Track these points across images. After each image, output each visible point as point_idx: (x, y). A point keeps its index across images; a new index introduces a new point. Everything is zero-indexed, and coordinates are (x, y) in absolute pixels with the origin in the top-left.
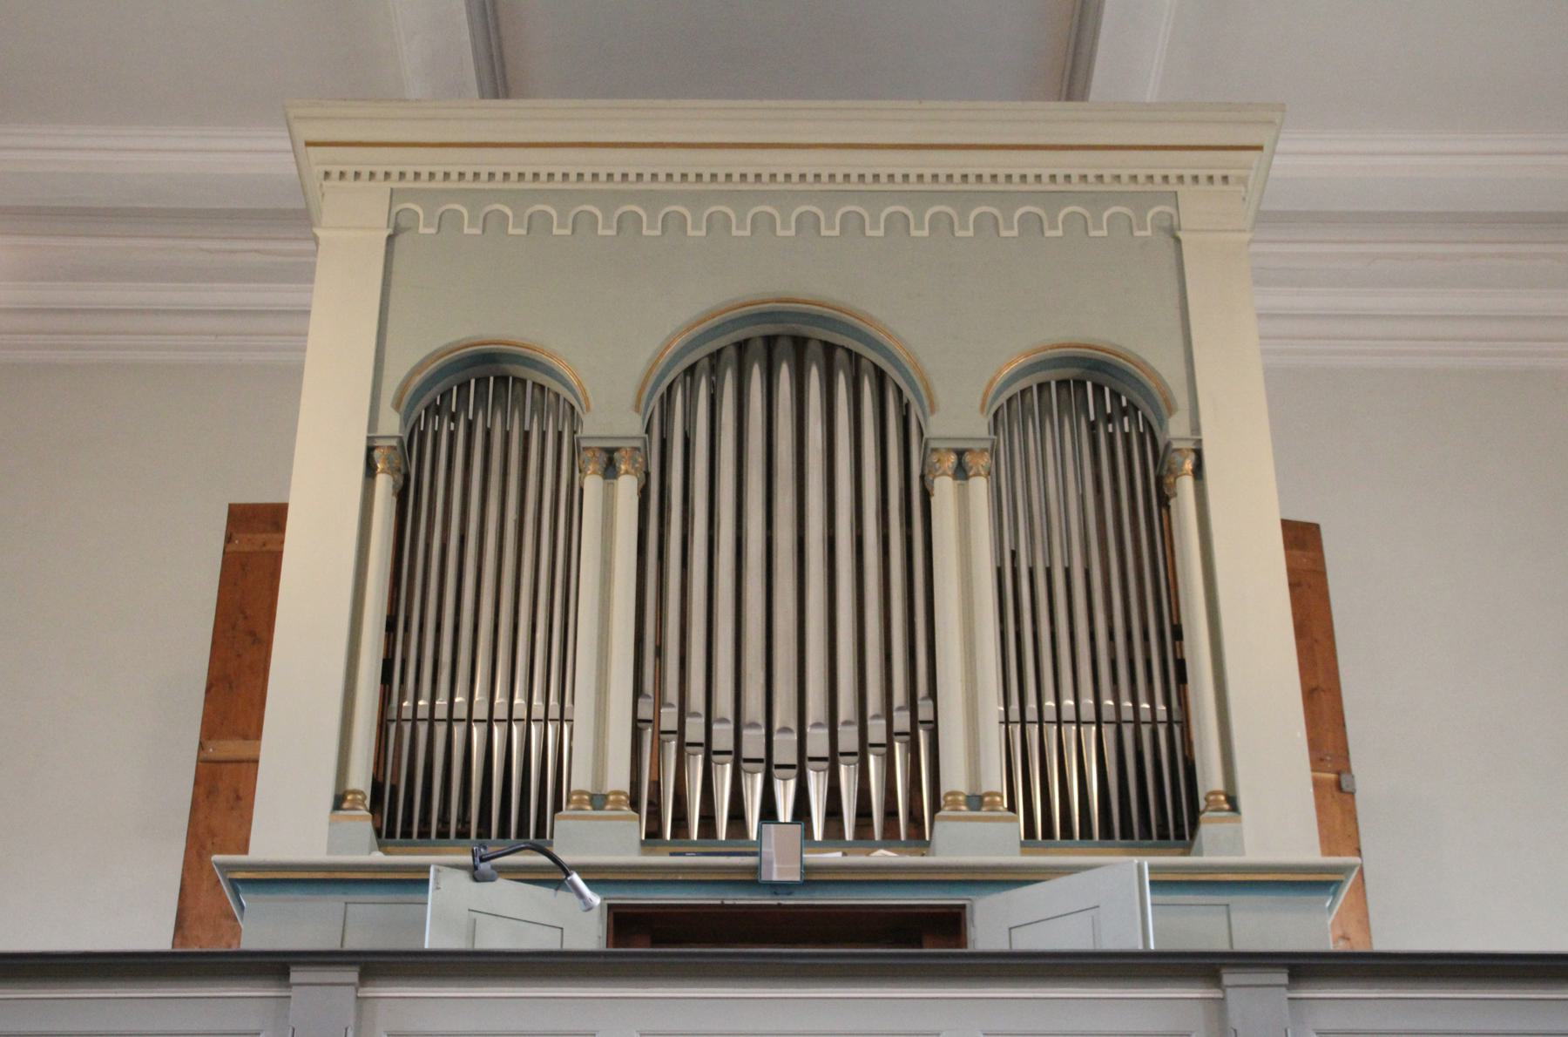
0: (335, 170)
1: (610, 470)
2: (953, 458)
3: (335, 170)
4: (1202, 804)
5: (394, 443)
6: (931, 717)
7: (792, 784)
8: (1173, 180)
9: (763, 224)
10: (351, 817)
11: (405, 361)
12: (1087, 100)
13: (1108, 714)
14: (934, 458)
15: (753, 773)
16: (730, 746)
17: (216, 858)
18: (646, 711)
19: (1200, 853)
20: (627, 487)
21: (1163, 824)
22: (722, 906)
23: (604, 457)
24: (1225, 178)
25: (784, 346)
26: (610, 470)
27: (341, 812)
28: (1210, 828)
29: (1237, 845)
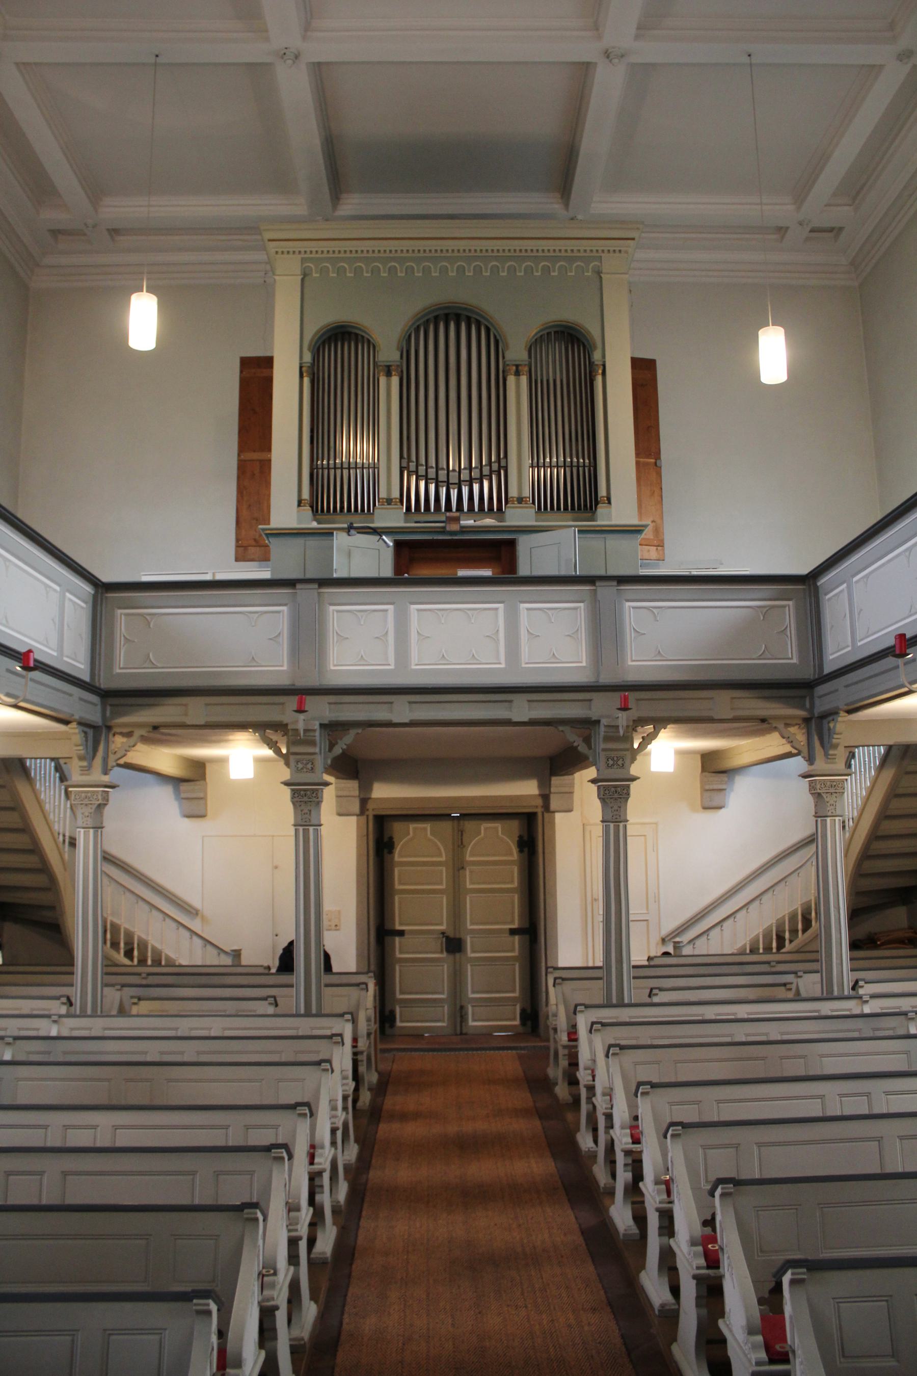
0: (280, 250)
1: (389, 374)
2: (514, 368)
3: (280, 250)
5: (309, 365)
6: (505, 465)
7: (456, 491)
8: (600, 251)
9: (443, 270)
10: (304, 510)
11: (311, 331)
13: (568, 464)
15: (443, 487)
16: (434, 477)
17: (261, 527)
18: (404, 464)
19: (596, 521)
20: (395, 380)
21: (585, 505)
22: (433, 539)
23: (386, 369)
26: (389, 374)
27: (301, 508)
28: (601, 510)
29: (609, 517)
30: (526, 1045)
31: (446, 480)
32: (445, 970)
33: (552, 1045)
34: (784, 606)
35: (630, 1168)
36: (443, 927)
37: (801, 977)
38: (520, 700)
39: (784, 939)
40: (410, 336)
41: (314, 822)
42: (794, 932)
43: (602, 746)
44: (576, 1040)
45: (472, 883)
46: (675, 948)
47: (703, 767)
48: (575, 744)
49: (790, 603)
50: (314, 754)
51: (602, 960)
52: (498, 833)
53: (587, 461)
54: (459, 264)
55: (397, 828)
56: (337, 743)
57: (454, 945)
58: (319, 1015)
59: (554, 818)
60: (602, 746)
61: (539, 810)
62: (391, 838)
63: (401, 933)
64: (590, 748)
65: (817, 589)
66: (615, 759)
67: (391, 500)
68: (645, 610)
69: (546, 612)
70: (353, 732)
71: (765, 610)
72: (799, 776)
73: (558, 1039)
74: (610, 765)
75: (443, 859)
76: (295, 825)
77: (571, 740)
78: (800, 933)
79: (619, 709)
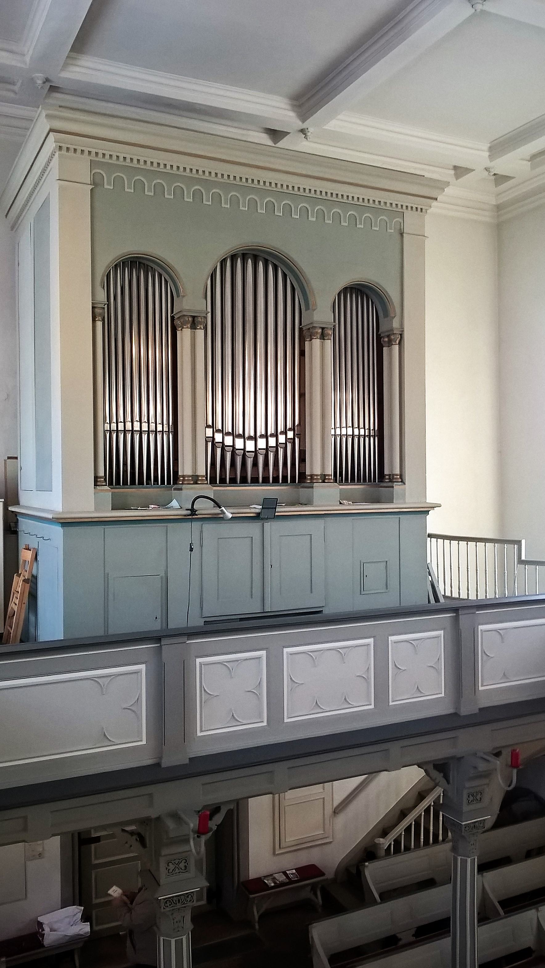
54: (250, 197)
68: (219, 665)
69: (498, 632)
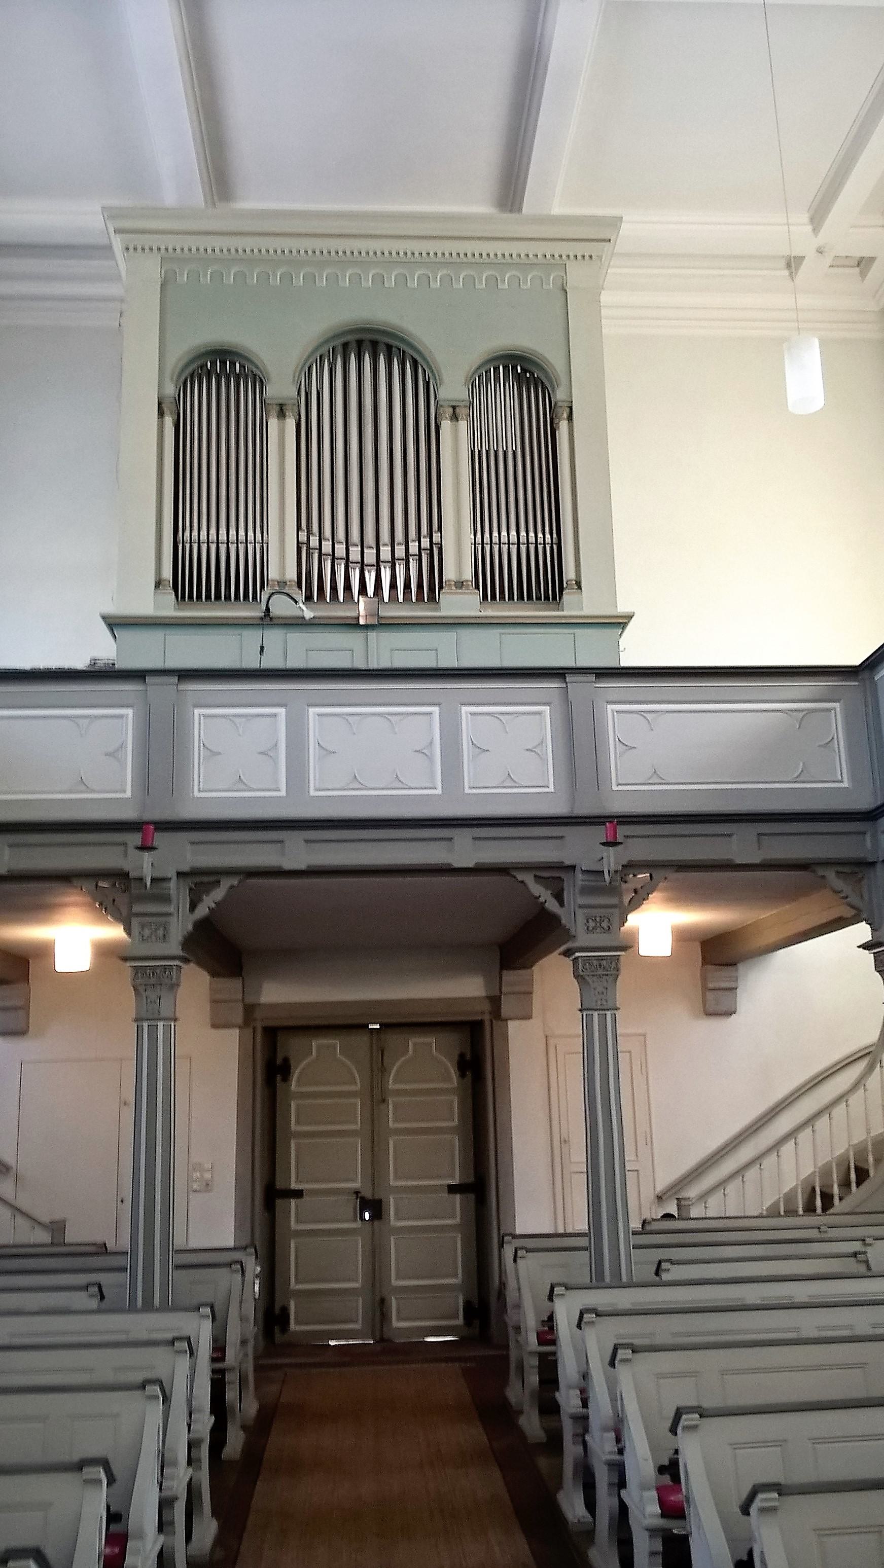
1: (282, 414)
2: (451, 410)
4: (565, 585)
7: (373, 574)
12: (520, 210)
14: (441, 410)
18: (303, 537)
20: (291, 423)
23: (278, 408)
24: (591, 257)
25: (367, 345)
26: (282, 414)
28: (568, 597)
29: (580, 603)
30: (472, 1354)
31: (359, 559)
32: (359, 1244)
33: (513, 1354)
34: (828, 710)
35: (659, 1559)
36: (357, 1185)
37: (870, 1245)
38: (462, 837)
39: (832, 1196)
40: (310, 368)
41: (165, 1012)
42: (845, 1184)
43: (581, 901)
44: (553, 1342)
45: (396, 1120)
46: (679, 1207)
47: (704, 958)
48: (542, 899)
49: (837, 705)
50: (169, 914)
51: (630, 1177)
52: (431, 1050)
53: (548, 536)
55: (292, 1046)
56: (201, 900)
57: (376, 1207)
58: (165, 1308)
59: (507, 1030)
60: (581, 901)
61: (487, 1018)
62: (286, 1060)
63: (298, 1194)
64: (561, 904)
65: (874, 684)
66: (598, 919)
67: (285, 583)
70: (226, 884)
71: (801, 715)
72: (859, 947)
73: (522, 1342)
74: (590, 929)
75: (357, 1087)
76: (136, 1020)
77: (537, 894)
78: (854, 1185)
79: (603, 844)
